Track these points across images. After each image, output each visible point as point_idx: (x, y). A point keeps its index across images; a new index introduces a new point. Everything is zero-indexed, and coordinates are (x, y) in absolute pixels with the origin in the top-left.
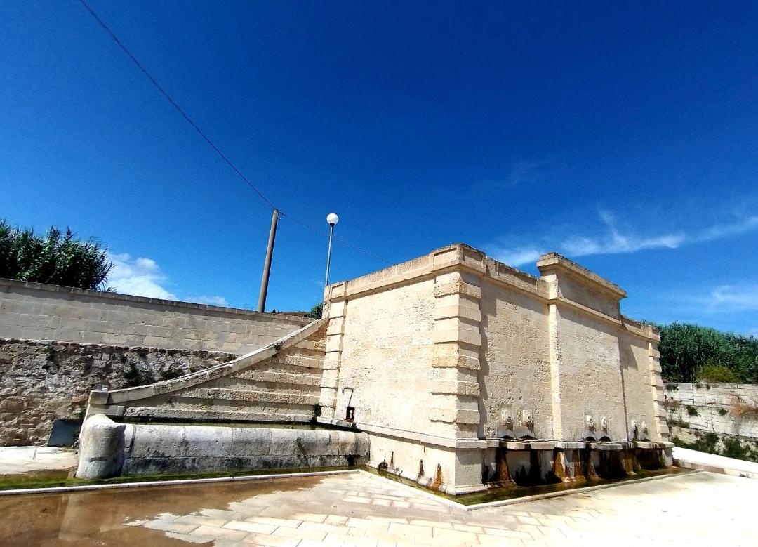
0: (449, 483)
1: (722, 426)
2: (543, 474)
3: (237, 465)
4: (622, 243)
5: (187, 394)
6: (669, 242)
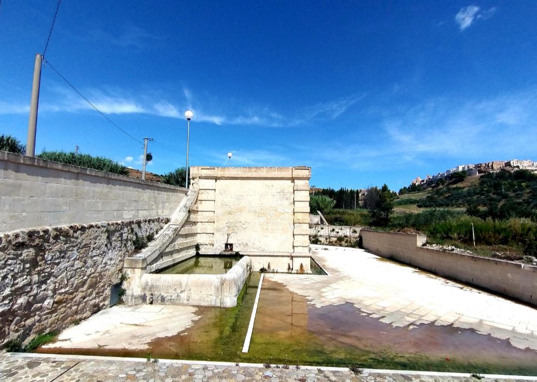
0: (308, 270)
5: (167, 250)
6: (217, 120)
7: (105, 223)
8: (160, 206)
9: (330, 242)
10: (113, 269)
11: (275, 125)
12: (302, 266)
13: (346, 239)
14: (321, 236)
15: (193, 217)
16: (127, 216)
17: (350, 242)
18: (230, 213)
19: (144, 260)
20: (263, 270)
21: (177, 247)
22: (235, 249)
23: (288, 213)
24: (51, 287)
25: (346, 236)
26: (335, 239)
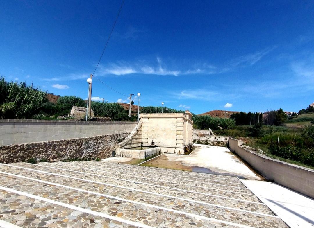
4: (162, 71)
6: (175, 73)
7: (110, 134)
8: (127, 129)
9: (213, 144)
10: (113, 147)
11: (211, 73)
12: (179, 151)
13: (221, 142)
14: (209, 141)
15: (139, 132)
16: (116, 133)
17: (223, 144)
18: (153, 131)
19: (121, 145)
20: (165, 152)
21: (132, 142)
23: (174, 131)
24: (99, 149)
25: (222, 141)
26: (216, 143)
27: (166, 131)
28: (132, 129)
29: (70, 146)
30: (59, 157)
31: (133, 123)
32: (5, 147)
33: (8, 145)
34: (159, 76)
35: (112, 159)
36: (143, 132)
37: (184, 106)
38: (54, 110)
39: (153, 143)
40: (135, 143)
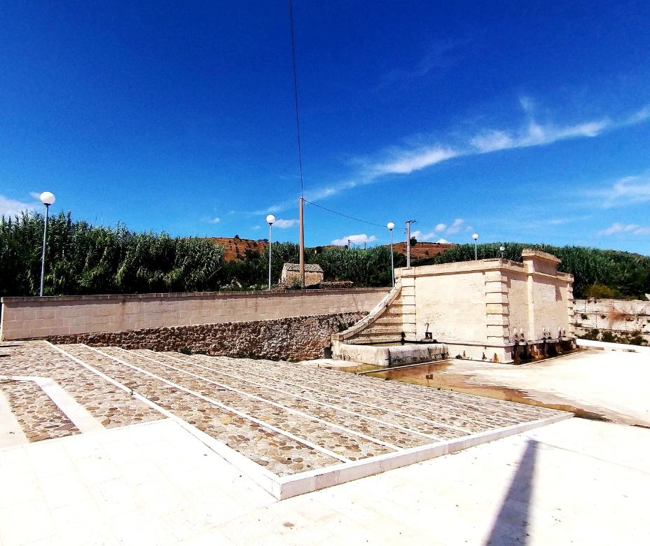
1: (602, 325)
2: (528, 354)
3: (415, 360)
4: (537, 134)
6: (589, 129)
12: (496, 355)
15: (392, 310)
16: (332, 311)
20: (458, 357)
21: (374, 332)
22: (434, 338)
23: (481, 304)
27: (450, 305)
28: (373, 303)
29: (240, 333)
30: (222, 349)
31: (378, 291)
32: (152, 330)
33: (157, 328)
34: (526, 149)
35: (323, 362)
36: (404, 310)
37: (630, 227)
38: (251, 269)
39: (428, 335)
40: (381, 334)
